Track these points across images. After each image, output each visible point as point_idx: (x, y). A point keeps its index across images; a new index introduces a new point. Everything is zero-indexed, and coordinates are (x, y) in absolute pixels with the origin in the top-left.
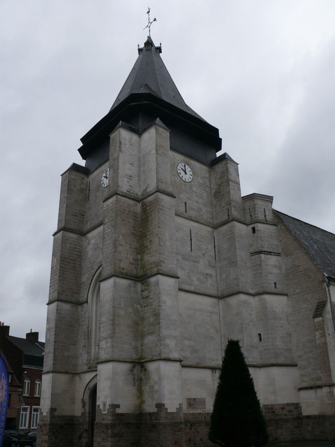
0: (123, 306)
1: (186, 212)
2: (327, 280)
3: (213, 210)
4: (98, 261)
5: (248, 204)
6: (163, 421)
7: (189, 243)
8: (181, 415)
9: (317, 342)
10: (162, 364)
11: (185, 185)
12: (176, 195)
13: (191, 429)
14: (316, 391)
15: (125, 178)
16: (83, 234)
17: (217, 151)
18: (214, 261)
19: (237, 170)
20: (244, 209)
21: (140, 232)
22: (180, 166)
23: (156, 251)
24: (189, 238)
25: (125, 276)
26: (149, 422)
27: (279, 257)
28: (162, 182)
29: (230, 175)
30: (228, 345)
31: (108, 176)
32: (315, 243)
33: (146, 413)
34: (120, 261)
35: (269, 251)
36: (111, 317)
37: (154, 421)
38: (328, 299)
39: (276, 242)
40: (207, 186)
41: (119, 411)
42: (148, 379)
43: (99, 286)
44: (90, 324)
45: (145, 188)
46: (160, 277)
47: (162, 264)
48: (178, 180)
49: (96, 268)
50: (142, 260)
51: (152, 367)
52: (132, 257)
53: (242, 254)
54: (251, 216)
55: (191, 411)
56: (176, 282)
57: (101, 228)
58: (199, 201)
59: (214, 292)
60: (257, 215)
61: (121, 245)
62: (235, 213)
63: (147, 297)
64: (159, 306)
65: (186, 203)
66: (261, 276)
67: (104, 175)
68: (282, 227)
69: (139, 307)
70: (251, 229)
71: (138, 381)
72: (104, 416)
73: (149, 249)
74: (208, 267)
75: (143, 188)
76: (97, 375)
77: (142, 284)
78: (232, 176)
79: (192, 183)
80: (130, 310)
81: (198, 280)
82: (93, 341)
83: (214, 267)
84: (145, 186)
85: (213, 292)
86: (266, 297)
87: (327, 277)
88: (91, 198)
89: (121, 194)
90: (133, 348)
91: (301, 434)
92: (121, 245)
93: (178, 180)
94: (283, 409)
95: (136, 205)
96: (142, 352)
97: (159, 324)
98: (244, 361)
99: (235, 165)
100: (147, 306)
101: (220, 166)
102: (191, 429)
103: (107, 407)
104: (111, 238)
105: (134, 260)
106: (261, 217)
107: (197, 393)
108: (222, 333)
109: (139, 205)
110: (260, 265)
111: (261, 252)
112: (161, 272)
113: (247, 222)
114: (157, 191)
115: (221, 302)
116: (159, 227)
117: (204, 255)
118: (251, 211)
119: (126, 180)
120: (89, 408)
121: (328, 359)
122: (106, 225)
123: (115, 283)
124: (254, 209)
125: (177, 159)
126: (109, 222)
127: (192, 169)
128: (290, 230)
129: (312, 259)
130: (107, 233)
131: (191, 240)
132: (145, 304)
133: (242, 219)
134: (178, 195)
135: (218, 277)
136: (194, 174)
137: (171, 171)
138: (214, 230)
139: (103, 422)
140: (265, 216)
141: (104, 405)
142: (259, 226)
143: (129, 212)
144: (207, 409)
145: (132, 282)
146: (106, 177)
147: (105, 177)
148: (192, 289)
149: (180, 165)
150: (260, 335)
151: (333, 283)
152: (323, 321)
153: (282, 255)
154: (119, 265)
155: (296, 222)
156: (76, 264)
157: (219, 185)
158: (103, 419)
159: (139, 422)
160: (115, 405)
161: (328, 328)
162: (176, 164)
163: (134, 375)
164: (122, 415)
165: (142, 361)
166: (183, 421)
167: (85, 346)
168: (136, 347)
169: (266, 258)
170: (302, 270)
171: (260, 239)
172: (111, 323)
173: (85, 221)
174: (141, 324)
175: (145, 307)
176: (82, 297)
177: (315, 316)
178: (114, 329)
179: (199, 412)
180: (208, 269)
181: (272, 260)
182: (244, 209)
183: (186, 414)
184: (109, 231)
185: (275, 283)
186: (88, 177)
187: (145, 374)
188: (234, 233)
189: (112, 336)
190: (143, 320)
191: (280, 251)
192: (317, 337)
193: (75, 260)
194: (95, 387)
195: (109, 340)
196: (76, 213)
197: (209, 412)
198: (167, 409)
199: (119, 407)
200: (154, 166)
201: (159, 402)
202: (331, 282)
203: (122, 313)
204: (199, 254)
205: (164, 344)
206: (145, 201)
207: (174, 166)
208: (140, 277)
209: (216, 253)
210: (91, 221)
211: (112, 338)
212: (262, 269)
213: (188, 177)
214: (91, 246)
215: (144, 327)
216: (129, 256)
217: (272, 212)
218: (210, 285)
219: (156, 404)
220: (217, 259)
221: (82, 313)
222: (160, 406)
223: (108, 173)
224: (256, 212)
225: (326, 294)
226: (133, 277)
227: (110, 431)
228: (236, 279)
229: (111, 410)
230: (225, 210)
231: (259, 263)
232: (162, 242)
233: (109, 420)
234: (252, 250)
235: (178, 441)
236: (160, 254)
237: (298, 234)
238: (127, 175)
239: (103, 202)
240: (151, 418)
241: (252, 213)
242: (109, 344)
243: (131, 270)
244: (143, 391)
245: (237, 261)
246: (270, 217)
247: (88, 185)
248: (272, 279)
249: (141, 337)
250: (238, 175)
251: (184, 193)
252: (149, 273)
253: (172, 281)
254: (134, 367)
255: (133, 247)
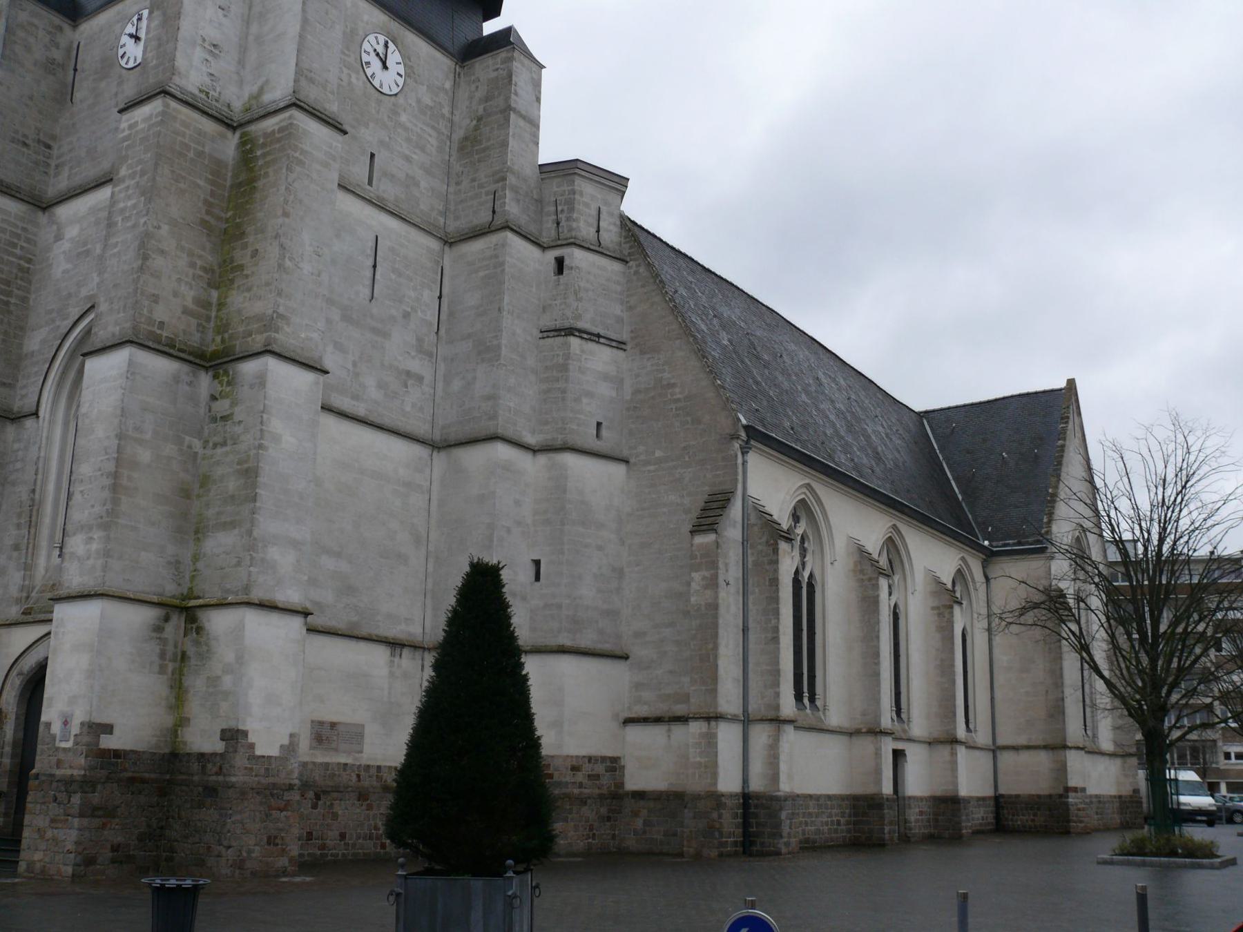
0: (148, 436)
1: (370, 183)
2: (743, 434)
3: (451, 190)
4: (84, 292)
5: (555, 188)
6: (237, 778)
7: (369, 273)
8: (294, 765)
9: (693, 599)
10: (253, 620)
11: (379, 102)
12: (346, 127)
13: (315, 806)
14: (669, 730)
15: (198, 49)
16: (43, 205)
17: (486, 19)
18: (433, 337)
19: (537, 84)
20: (540, 201)
21: (227, 221)
22: (374, 42)
23: (267, 284)
24: (370, 262)
25: (166, 349)
26: (196, 778)
27: (621, 353)
28: (312, 81)
29: (516, 94)
30: (467, 574)
31: (142, 35)
32: (724, 327)
33: (189, 754)
34: (155, 299)
35: (595, 330)
36: (111, 466)
37: (214, 778)
38: (740, 486)
39: (617, 310)
40: (443, 116)
41: (108, 742)
42: (205, 655)
43: (81, 372)
44: (39, 483)
45: (255, 89)
46: (271, 362)
47: (280, 323)
48: (358, 81)
49: (75, 313)
50: (221, 305)
51: (218, 622)
52: (192, 293)
53: (517, 330)
54: (558, 224)
55: (321, 758)
56: (317, 383)
57: (104, 193)
58: (413, 156)
59: (422, 429)
60: (574, 225)
61: (162, 252)
62: (512, 208)
63: (224, 418)
64: (260, 447)
65: (372, 155)
66: (563, 399)
67: (130, 29)
68: (642, 270)
69: (197, 444)
70: (553, 261)
71: (174, 660)
72: (61, 756)
73: (247, 276)
74: (413, 354)
75: (250, 89)
76: (49, 633)
77: (215, 377)
78: (521, 101)
79: (401, 100)
80: (170, 449)
81: (381, 385)
82: (45, 531)
83: (430, 355)
84: (259, 83)
85: (420, 427)
86: (569, 459)
87: (746, 428)
88: (78, 95)
89: (178, 94)
90: (169, 563)
91: (614, 837)
92: (162, 252)
93: (361, 83)
94: (575, 769)
95: (223, 137)
96: (193, 578)
97: (254, 500)
98: (510, 625)
99: (534, 67)
100: (224, 444)
101: (490, 62)
102: (315, 806)
103: (75, 729)
104: (134, 226)
105: (198, 301)
106: (586, 231)
107: (342, 708)
108: (431, 548)
109: (233, 139)
110: (564, 368)
111: (570, 331)
112: (277, 349)
113: (544, 240)
114: (294, 105)
115: (440, 459)
116: (286, 214)
117: (406, 315)
118: (560, 208)
119: (199, 54)
120: (16, 731)
121: (716, 647)
122: (122, 186)
123: (131, 363)
124: (571, 204)
125: (366, 18)
126: (132, 176)
127: (406, 58)
128: (661, 281)
129: (713, 373)
130: (123, 210)
131: (375, 266)
132: (216, 439)
133: (532, 229)
134: (354, 127)
135: (440, 385)
136: (410, 73)
137: (343, 53)
138: (446, 248)
139: (58, 772)
140: (598, 231)
141: (66, 723)
142: (577, 257)
143: (200, 154)
144: (364, 755)
145: (185, 368)
146: (136, 38)
147: (131, 36)
148: (361, 410)
149: (371, 38)
150: (537, 563)
151: (759, 445)
152: (718, 545)
153: (628, 347)
154: (151, 311)
155: (681, 261)
156: (9, 294)
157: (479, 119)
158: (59, 764)
159: (168, 777)
160: (99, 725)
161: (726, 565)
162: (361, 33)
163: (163, 641)
164: (117, 754)
165: (192, 603)
166: (297, 782)
167: (16, 547)
168: (178, 562)
169: (583, 351)
170: (679, 396)
171: (576, 294)
172: (107, 482)
173: (53, 164)
174: (199, 496)
175: (215, 446)
176: (23, 397)
177: (697, 530)
178: (115, 501)
179: (343, 760)
180: (413, 358)
181: (600, 358)
182: (540, 201)
183: (304, 764)
184: (129, 203)
185: (599, 424)
186: (75, 27)
187: (197, 643)
188: (502, 264)
189: (108, 521)
190: (207, 485)
191: (625, 337)
192: (694, 586)
193: (8, 283)
194: (41, 668)
195: (97, 534)
196: (25, 136)
197: (371, 763)
198: (252, 746)
199: (111, 733)
200: (293, 27)
201: (232, 724)
202: (752, 442)
203: (145, 456)
204: (394, 312)
205: (263, 560)
206: (252, 128)
207: (353, 40)
208: (213, 357)
209: (443, 317)
210: (71, 168)
211: (106, 527)
212: (567, 380)
213: (389, 80)
214: (65, 245)
215: (207, 505)
216: (183, 288)
217: (618, 223)
218: (414, 405)
219: (223, 731)
220: (442, 331)
221: (16, 446)
222: (233, 736)
223: (144, 23)
224: (575, 215)
225: (736, 473)
226: (190, 354)
227: (76, 799)
228: (492, 397)
229: (86, 739)
230: (487, 194)
231: (561, 361)
232: (291, 259)
233: (77, 767)
234: (547, 321)
235: (276, 837)
236: (280, 294)
237: (682, 296)
238: (204, 40)
239: (120, 111)
240: (204, 767)
241: (562, 217)
242: (94, 546)
243: (184, 331)
244: (186, 691)
245: (499, 346)
246: (611, 234)
247: (74, 52)
248: (591, 410)
249: (197, 532)
250: (538, 100)
251: (371, 125)
252: (239, 347)
253: (305, 378)
254: (167, 619)
255: (199, 263)
